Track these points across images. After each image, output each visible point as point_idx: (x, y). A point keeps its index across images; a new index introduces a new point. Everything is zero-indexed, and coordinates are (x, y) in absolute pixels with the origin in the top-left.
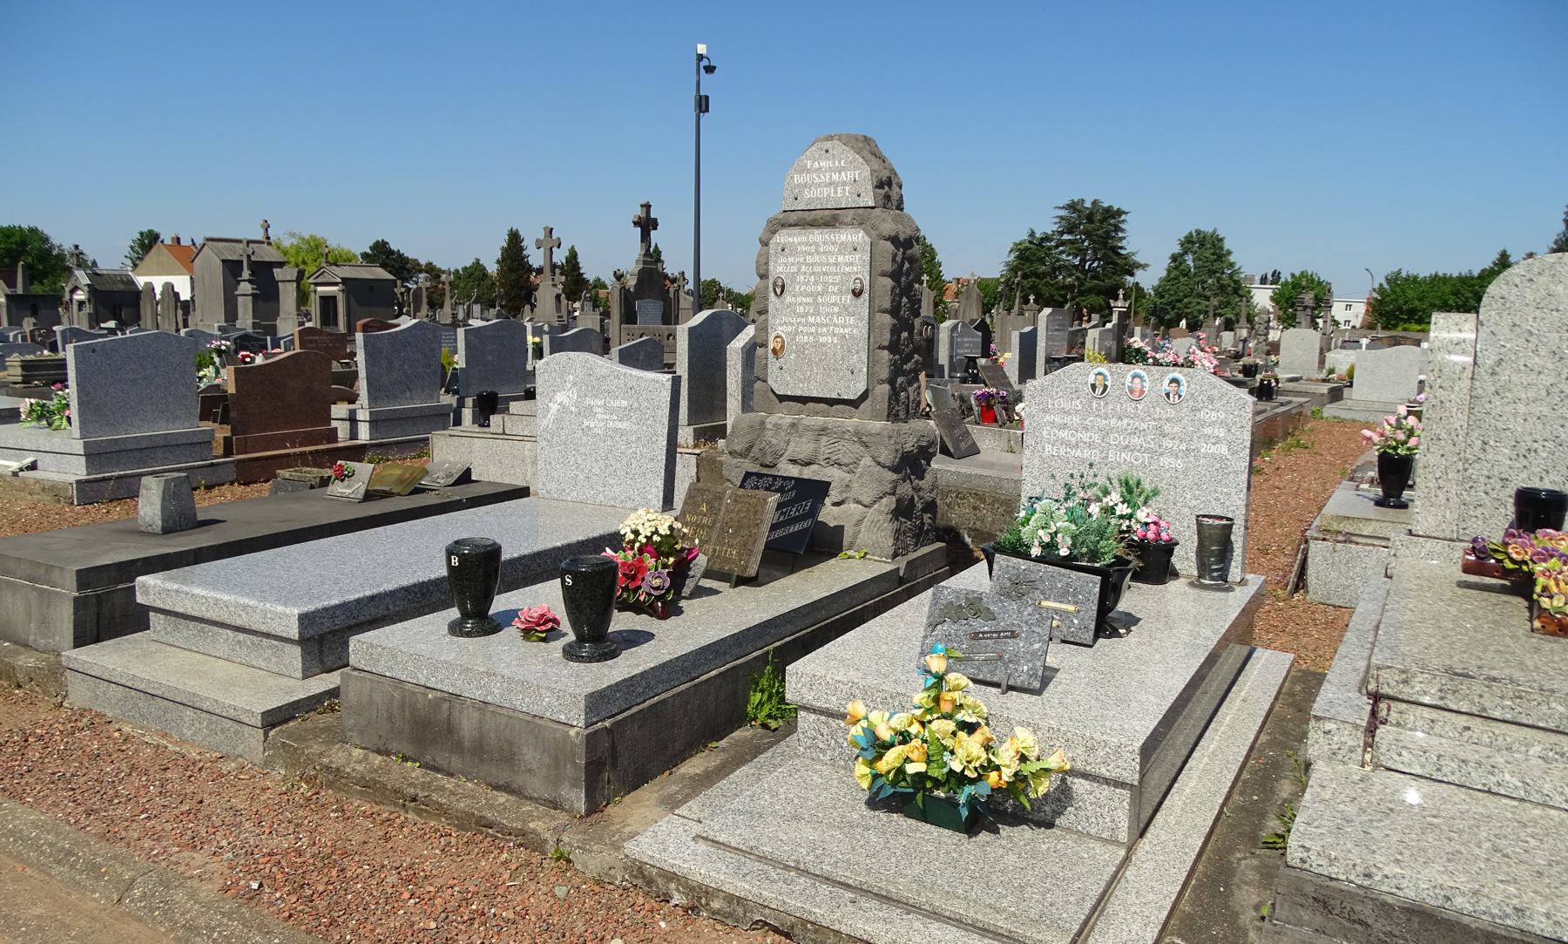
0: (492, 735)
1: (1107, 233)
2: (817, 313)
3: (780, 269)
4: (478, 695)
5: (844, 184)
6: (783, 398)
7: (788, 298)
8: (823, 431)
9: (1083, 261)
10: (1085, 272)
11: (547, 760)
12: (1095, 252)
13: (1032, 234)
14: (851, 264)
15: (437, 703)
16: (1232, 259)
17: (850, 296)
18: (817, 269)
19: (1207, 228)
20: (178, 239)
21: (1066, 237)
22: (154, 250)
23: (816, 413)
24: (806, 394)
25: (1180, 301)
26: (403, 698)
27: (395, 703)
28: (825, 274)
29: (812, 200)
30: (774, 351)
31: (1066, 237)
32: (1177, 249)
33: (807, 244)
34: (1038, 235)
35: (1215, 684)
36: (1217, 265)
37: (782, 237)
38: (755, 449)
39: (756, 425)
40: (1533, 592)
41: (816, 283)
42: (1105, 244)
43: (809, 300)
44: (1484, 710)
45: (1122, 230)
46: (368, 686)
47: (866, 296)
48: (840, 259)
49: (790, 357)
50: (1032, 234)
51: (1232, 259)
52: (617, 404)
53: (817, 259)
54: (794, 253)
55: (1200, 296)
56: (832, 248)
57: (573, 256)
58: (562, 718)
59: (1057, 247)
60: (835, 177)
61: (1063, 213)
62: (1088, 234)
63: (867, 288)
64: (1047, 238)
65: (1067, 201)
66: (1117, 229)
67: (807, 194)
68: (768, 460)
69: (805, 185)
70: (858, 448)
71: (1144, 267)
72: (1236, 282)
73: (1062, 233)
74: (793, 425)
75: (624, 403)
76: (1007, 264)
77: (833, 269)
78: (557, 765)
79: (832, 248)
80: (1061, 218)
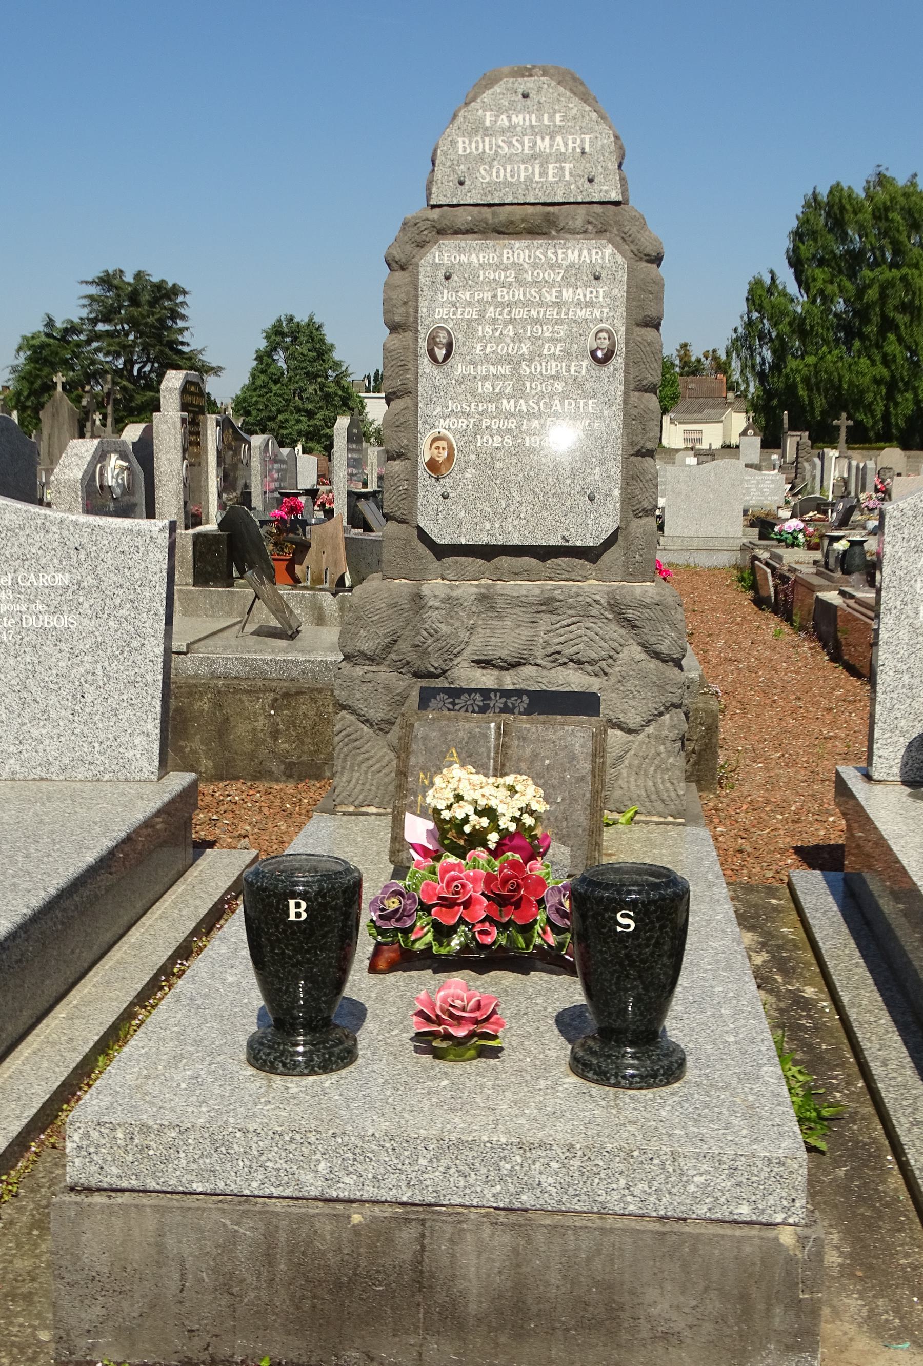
0: (554, 1277)
1: (162, 321)
2: (519, 393)
3: (441, 313)
4: (491, 1195)
5: (561, 158)
6: (441, 551)
7: (459, 367)
8: (548, 604)
9: (130, 363)
10: (134, 381)
11: (714, 1305)
12: (145, 349)
13: (50, 323)
14: (590, 304)
15: (380, 1234)
17: (586, 363)
18: (517, 313)
21: (101, 327)
23: (516, 575)
24: (499, 540)
25: (272, 419)
26: (270, 1235)
27: (242, 1252)
28: (537, 321)
29: (496, 186)
30: (433, 465)
31: (101, 327)
32: (263, 344)
33: (498, 267)
34: (59, 324)
36: (318, 366)
37: (445, 253)
38: (404, 646)
39: (404, 602)
41: (518, 338)
42: (159, 338)
43: (505, 370)
45: (183, 317)
46: (151, 1223)
47: (618, 361)
48: (567, 294)
49: (463, 476)
50: (50, 323)
52: (45, 580)
53: (519, 294)
54: (471, 281)
55: (298, 410)
56: (549, 275)
58: (744, 1211)
59: (89, 342)
60: (543, 144)
61: (94, 290)
62: (134, 323)
63: (620, 347)
64: (72, 329)
65: (96, 273)
66: (175, 315)
67: (485, 176)
68: (434, 662)
69: (481, 158)
70: (615, 631)
71: (216, 371)
72: (343, 388)
73: (94, 321)
74: (483, 598)
75: (62, 579)
76: (14, 370)
77: (553, 313)
78: (746, 1314)
79: (549, 275)
80: (91, 298)
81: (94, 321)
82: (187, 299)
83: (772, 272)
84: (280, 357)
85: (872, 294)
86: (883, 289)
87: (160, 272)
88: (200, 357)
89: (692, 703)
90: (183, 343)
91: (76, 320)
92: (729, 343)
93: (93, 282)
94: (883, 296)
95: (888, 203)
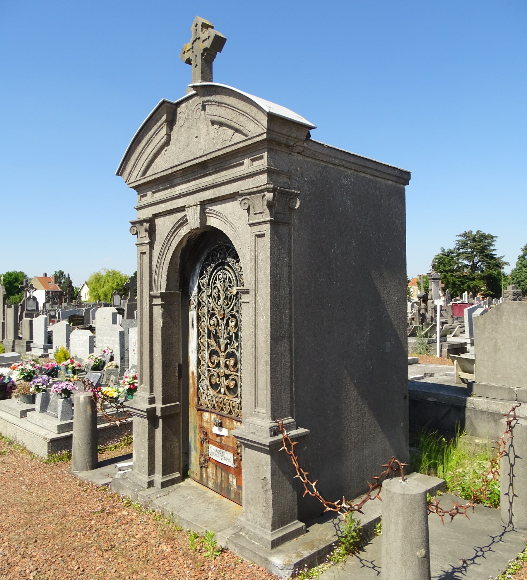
20: (46, 274)
25: (522, 281)
31: (461, 251)
34: (446, 251)
35: (164, 213)
45: (493, 245)
57: (495, 240)
64: (450, 252)
71: (507, 264)
73: (459, 249)
80: (459, 241)
81: (459, 249)
82: (497, 239)
87: (486, 231)
88: (502, 260)
89: (266, 533)
90: (495, 255)
91: (452, 249)
93: (460, 236)
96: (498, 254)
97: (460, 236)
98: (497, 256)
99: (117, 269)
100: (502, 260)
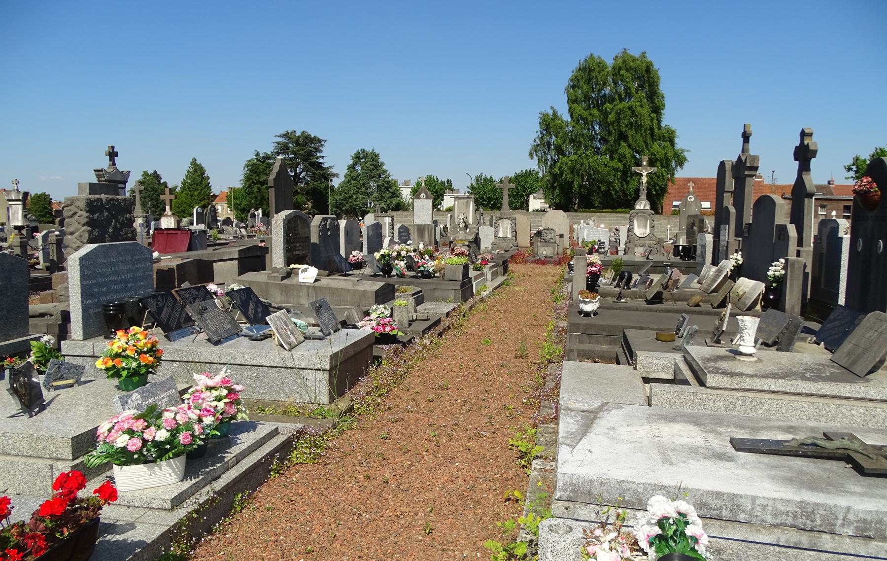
13: (258, 154)
16: (385, 168)
19: (368, 149)
22: (561, 416)
25: (351, 197)
32: (351, 162)
40: (380, 344)
44: (278, 372)
50: (258, 154)
51: (385, 168)
61: (281, 140)
71: (336, 175)
72: (388, 182)
80: (278, 143)
83: (552, 108)
84: (359, 168)
85: (611, 117)
86: (618, 114)
88: (331, 170)
91: (269, 153)
92: (531, 147)
93: (280, 136)
94: (618, 119)
95: (569, 251)
96: (327, 162)
97: (280, 136)
98: (325, 166)
99: (677, 133)
100: (331, 170)
